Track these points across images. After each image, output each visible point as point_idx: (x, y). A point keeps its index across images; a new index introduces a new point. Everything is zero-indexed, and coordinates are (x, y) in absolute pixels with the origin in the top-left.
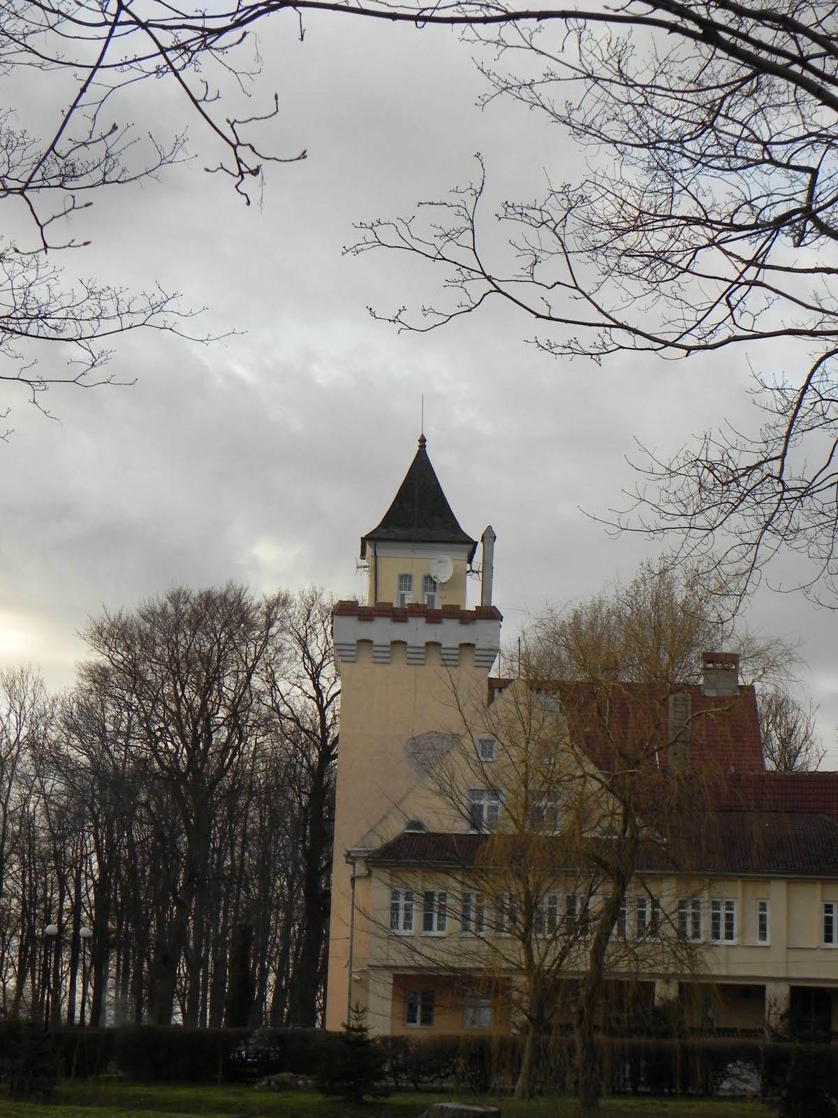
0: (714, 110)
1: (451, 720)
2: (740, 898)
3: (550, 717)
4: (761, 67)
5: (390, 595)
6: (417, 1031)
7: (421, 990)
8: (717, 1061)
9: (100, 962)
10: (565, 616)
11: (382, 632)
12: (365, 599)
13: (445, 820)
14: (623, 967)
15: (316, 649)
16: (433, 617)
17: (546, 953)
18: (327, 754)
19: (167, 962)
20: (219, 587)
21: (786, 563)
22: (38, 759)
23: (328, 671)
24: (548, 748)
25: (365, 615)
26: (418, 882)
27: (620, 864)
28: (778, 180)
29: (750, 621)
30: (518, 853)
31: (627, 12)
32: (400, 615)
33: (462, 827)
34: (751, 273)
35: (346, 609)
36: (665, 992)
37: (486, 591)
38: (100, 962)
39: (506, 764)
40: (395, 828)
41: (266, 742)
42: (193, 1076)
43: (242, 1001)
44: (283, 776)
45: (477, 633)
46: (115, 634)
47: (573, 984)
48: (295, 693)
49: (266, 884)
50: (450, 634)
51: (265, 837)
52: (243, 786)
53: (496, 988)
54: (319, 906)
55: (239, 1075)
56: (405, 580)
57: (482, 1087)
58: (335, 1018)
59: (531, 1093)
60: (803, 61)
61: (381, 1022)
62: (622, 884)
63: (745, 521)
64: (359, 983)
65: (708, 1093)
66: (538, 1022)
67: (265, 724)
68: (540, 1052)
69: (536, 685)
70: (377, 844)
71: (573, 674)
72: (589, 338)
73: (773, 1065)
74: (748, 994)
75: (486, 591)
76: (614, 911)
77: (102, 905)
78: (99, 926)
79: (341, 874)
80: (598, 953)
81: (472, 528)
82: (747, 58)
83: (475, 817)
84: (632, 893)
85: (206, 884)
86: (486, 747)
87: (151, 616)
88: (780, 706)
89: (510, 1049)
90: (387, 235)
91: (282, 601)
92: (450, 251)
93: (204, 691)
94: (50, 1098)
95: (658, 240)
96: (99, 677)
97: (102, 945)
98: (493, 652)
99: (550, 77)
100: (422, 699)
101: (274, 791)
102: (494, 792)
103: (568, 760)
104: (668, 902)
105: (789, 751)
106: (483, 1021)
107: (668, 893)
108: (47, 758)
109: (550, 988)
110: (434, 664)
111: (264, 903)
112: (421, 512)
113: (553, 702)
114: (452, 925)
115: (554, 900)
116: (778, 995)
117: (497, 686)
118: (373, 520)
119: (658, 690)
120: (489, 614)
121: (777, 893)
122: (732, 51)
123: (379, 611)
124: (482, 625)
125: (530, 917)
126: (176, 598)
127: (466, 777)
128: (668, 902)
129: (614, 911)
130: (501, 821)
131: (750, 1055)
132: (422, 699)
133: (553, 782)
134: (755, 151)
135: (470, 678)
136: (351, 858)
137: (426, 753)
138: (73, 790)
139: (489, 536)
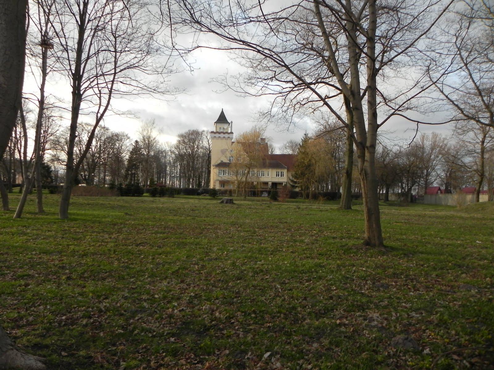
0: (261, 62)
1: (226, 147)
2: (265, 171)
3: (240, 147)
4: (266, 57)
5: (218, 130)
6: (222, 188)
7: (223, 183)
8: (262, 192)
9: (180, 179)
10: (242, 133)
11: (217, 135)
12: (215, 131)
13: (226, 161)
14: (250, 180)
15: (208, 138)
16: (224, 133)
17: (239, 178)
18: (210, 152)
19: (189, 180)
20: (195, 129)
21: (271, 126)
22: (171, 152)
23: (210, 141)
24: (240, 151)
25: (215, 133)
26: (223, 169)
27: (250, 166)
28: (270, 72)
29: (266, 135)
30: (236, 165)
31: (50, 28)
32: (220, 133)
33: (228, 162)
34: (266, 85)
35: (212, 132)
36: (255, 183)
37: (231, 130)
38: (180, 179)
39: (234, 153)
40: (219, 162)
41: (202, 150)
42: (193, 194)
43: (199, 185)
44: (204, 155)
45: (230, 135)
46: (181, 136)
47: (243, 182)
48: (205, 144)
49: (202, 169)
50: (226, 136)
51: (202, 163)
52: (199, 156)
53: (233, 183)
54: (209, 173)
55: (199, 194)
56: (220, 128)
57: (231, 195)
58: (211, 187)
59: (238, 196)
60: (271, 55)
61: (218, 187)
62: (249, 169)
63: (266, 120)
64: (215, 182)
65: (260, 196)
66: (238, 187)
67: (202, 148)
68: (238, 191)
69: (238, 142)
70: (216, 164)
71: (243, 141)
72: (243, 94)
73: (269, 193)
74: (266, 183)
75: (231, 130)
76: (248, 172)
77: (180, 172)
78: (180, 175)
79: (212, 168)
80: (246, 178)
81: (229, 121)
82: (264, 55)
83: (230, 160)
84: (251, 170)
85: (194, 169)
86: (231, 151)
87: (186, 133)
88: (271, 146)
89: (235, 190)
90: (214, 80)
91: (204, 131)
92: (223, 82)
93: (193, 143)
94: (173, 197)
95: (253, 81)
96: (179, 142)
97: (180, 177)
98: (232, 138)
99: (237, 57)
100: (223, 144)
101: (203, 157)
102: (232, 157)
103: (242, 153)
104: (256, 171)
105: (272, 152)
106: (231, 187)
107: (256, 171)
108: (172, 152)
109: (240, 183)
110: (224, 140)
111: (202, 172)
112: (222, 119)
113: (240, 145)
114: (227, 174)
115: (241, 171)
116: (270, 184)
117: (233, 143)
118: (216, 121)
119: (254, 143)
120: (232, 133)
121: (270, 170)
122: (262, 54)
123: (217, 132)
124: (231, 135)
125: (237, 174)
126: (189, 131)
127: (228, 155)
128: (256, 171)
129: (248, 172)
130: (234, 161)
131: (266, 191)
132: (223, 144)
133: (240, 155)
134: (267, 69)
135: (229, 142)
136: (213, 166)
137: (223, 152)
138: (176, 157)
139: (232, 122)
